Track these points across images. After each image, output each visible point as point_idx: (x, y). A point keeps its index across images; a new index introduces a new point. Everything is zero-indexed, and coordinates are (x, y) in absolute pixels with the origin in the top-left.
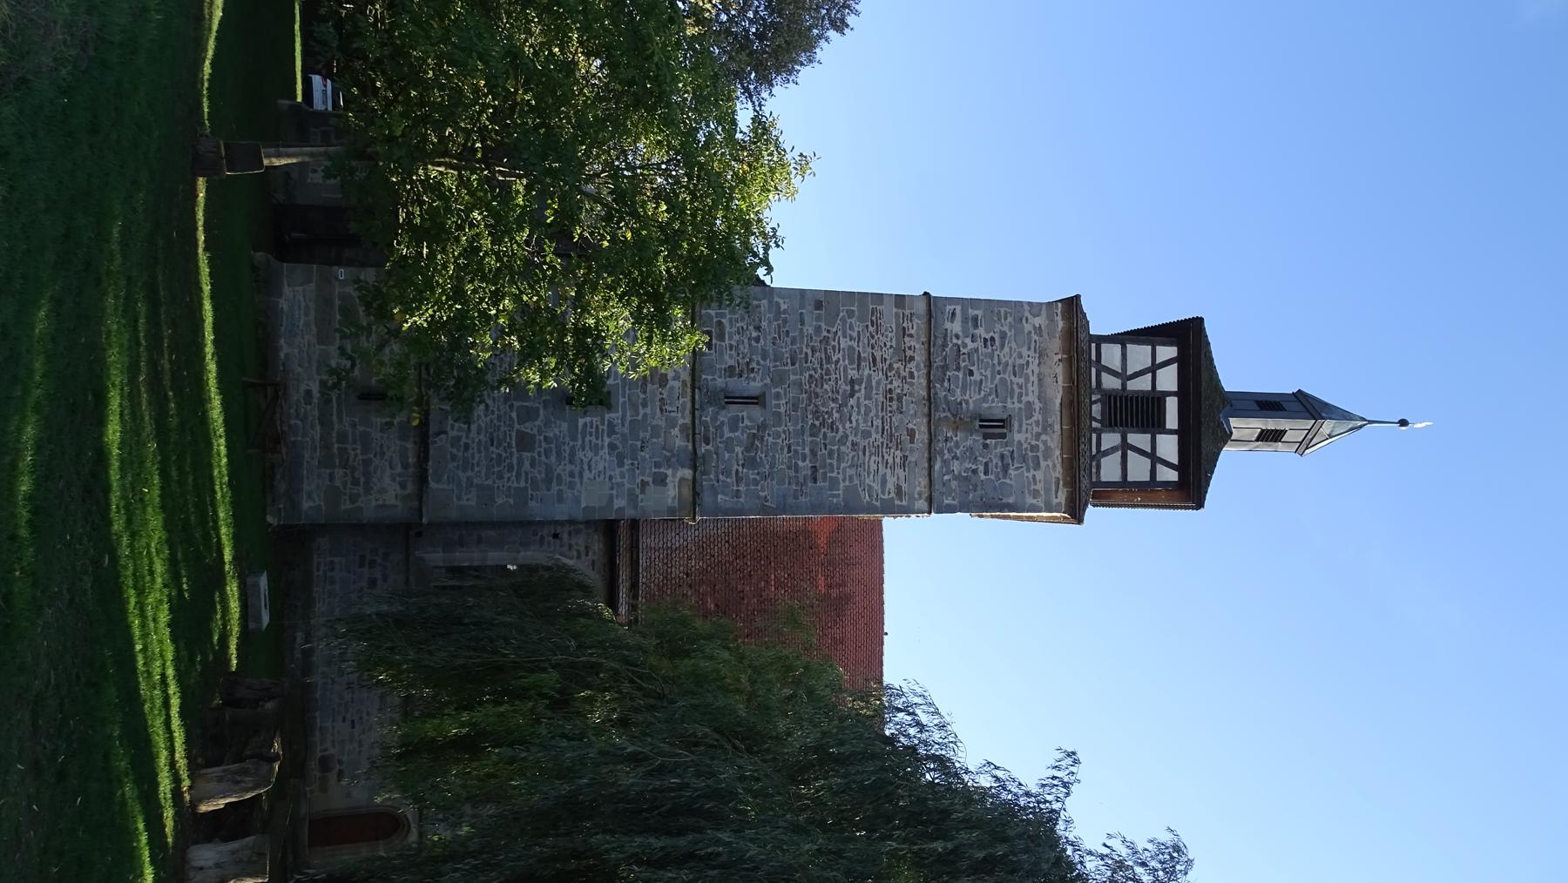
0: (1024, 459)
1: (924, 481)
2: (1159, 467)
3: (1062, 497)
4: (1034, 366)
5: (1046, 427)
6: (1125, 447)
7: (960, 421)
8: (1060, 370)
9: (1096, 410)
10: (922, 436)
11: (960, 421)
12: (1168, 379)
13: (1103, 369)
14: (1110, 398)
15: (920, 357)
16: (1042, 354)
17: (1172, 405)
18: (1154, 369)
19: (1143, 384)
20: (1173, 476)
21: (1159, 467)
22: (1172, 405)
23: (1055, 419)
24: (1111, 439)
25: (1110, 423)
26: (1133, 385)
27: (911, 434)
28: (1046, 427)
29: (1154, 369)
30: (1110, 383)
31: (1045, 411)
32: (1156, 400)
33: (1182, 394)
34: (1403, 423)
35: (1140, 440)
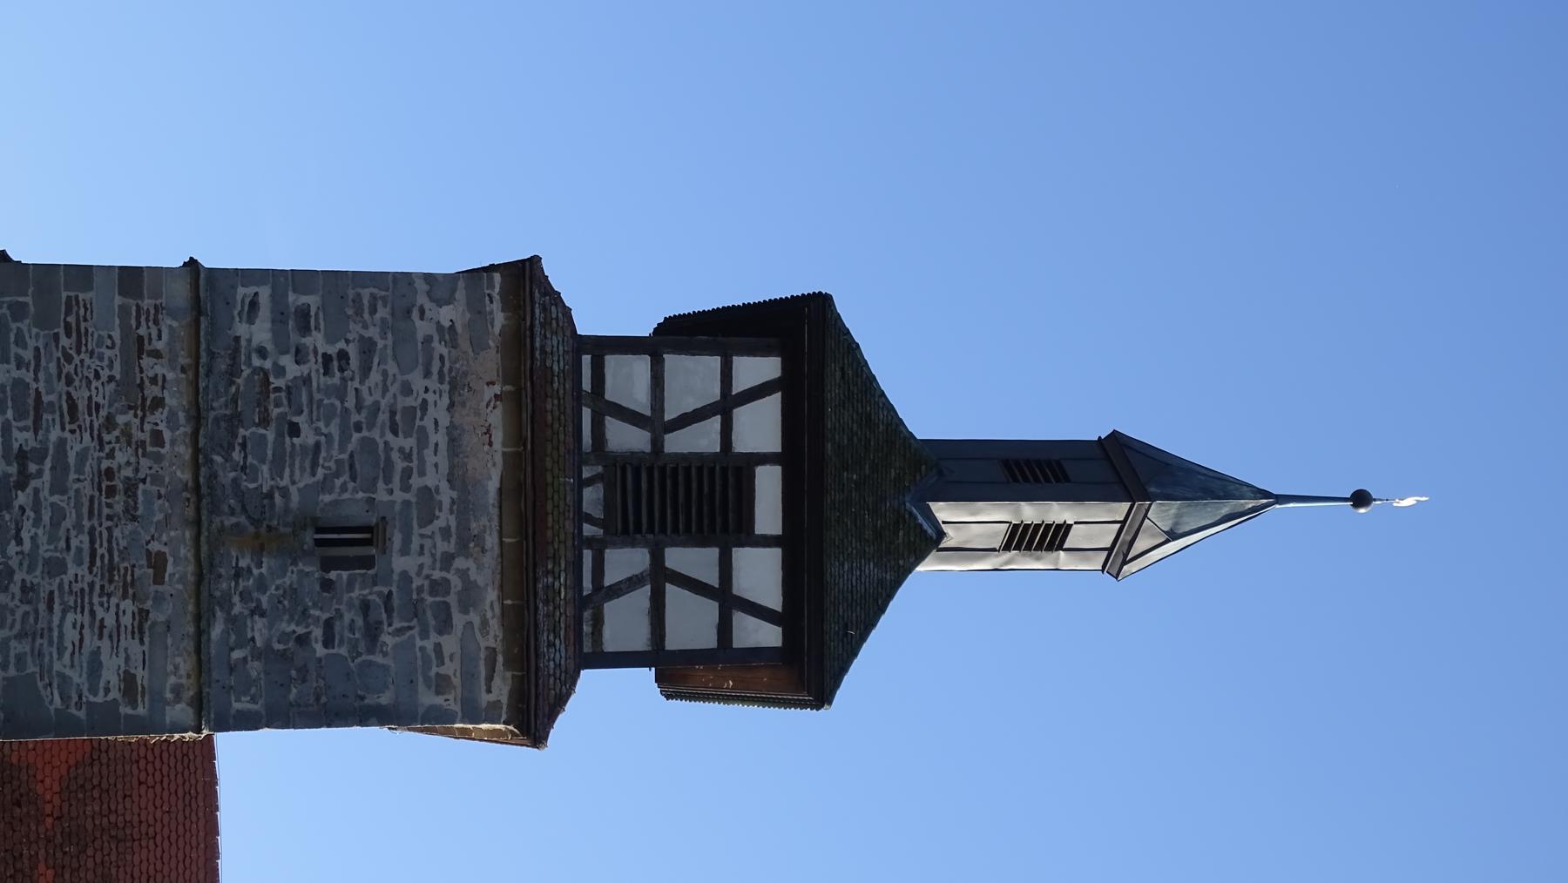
0: (415, 610)
1: (185, 664)
2: (712, 578)
3: (501, 690)
4: (439, 411)
5: (467, 541)
6: (659, 576)
7: (269, 531)
8: (496, 417)
9: (592, 497)
10: (180, 568)
11: (269, 531)
12: (759, 428)
13: (606, 409)
14: (621, 469)
15: (175, 400)
16: (456, 385)
17: (768, 485)
18: (726, 405)
19: (703, 439)
20: (769, 636)
21: (712, 578)
22: (768, 485)
23: (489, 528)
24: (625, 561)
25: (622, 528)
26: (679, 443)
27: (158, 563)
28: (467, 541)
29: (726, 405)
30: (625, 438)
31: (463, 507)
32: (735, 471)
33: (796, 455)
34: (1360, 499)
35: (696, 561)
